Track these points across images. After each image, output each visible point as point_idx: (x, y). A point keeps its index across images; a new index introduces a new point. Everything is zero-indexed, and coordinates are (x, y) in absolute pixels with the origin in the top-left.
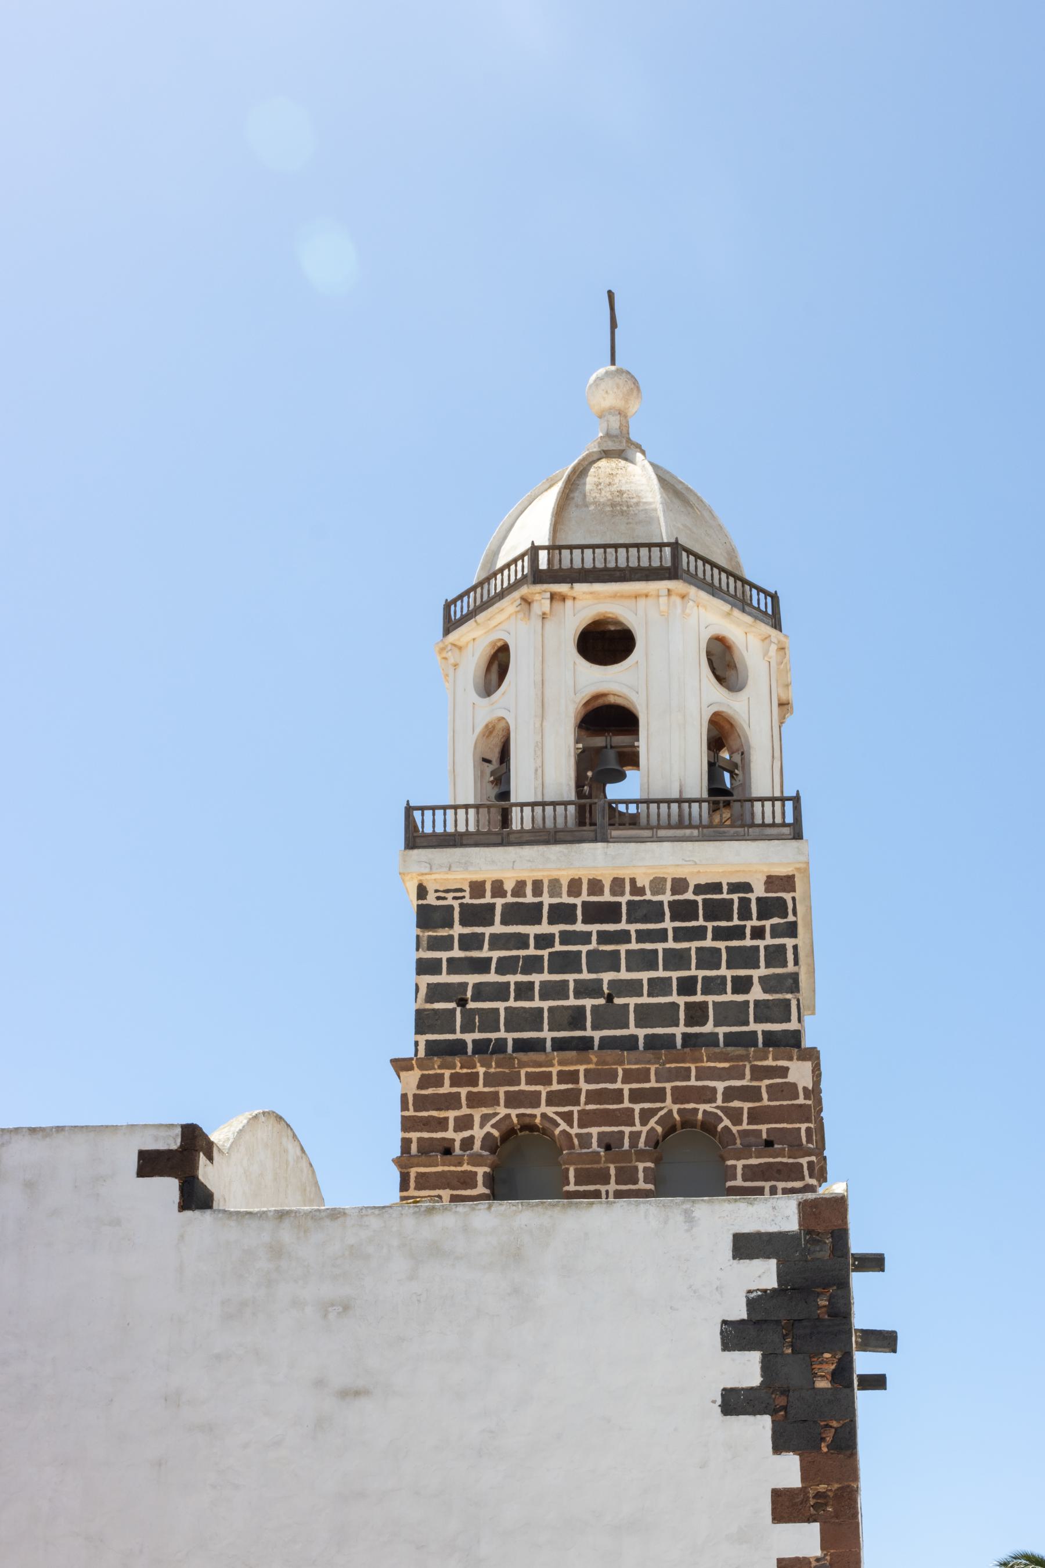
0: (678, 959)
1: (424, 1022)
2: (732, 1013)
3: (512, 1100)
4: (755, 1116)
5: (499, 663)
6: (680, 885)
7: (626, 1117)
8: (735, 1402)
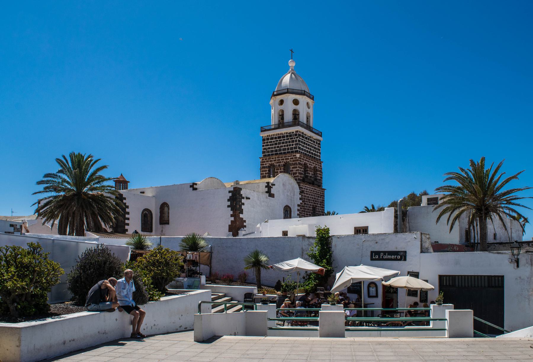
0: (286, 142)
1: (263, 152)
2: (292, 148)
3: (271, 161)
4: (293, 161)
5: (282, 102)
6: (287, 133)
7: (280, 162)
8: (228, 206)
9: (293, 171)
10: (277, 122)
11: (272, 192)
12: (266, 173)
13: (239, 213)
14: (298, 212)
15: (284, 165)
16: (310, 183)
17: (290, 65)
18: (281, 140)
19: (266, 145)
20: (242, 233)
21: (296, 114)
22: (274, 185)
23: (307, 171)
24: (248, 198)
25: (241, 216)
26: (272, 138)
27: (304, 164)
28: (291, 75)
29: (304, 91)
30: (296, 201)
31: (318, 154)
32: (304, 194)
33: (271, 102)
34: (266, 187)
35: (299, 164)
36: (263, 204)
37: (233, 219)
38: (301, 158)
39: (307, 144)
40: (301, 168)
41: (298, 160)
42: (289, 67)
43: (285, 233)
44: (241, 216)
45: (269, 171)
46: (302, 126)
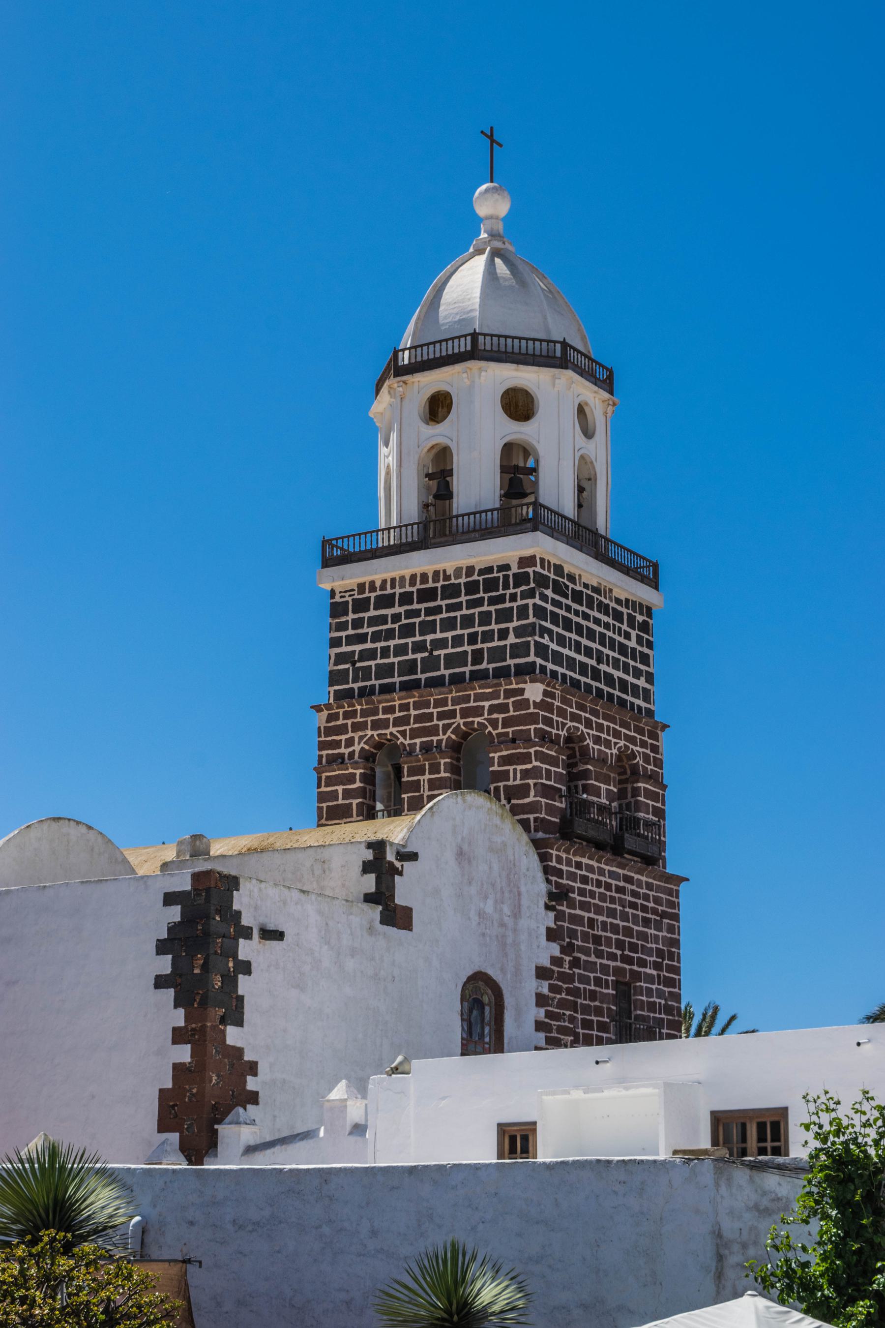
0: (468, 621)
1: (335, 678)
2: (497, 654)
3: (376, 725)
4: (507, 723)
5: (438, 407)
6: (470, 570)
7: (434, 731)
8: (160, 982)
9: (505, 776)
10: (413, 513)
11: (400, 900)
12: (347, 794)
13: (223, 1020)
14: (542, 1012)
15: (455, 748)
16: (600, 846)
17: (482, 210)
18: (438, 610)
19: (351, 640)
20: (235, 1134)
21: (517, 473)
22: (413, 857)
23: (585, 774)
24: (272, 935)
25: (233, 1036)
26: (386, 601)
27: (569, 739)
28: (491, 263)
29: (565, 345)
30: (527, 949)
31: (642, 682)
32: (572, 904)
33: (381, 406)
34: (367, 868)
35: (544, 737)
36: (350, 964)
37: (184, 1054)
38: (548, 707)
39: (579, 630)
40: (554, 762)
41: (533, 719)
42: (480, 220)
43: (517, 1140)
44: (233, 1036)
45: (375, 781)
46: (554, 532)
